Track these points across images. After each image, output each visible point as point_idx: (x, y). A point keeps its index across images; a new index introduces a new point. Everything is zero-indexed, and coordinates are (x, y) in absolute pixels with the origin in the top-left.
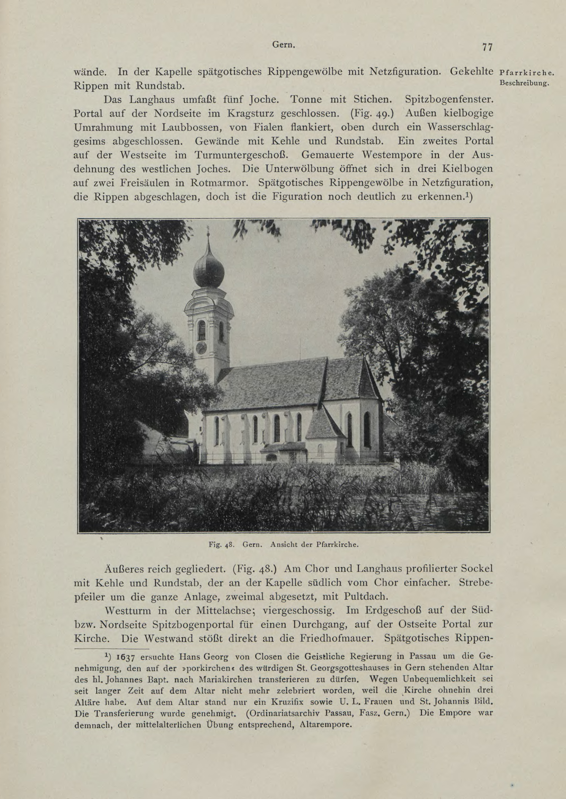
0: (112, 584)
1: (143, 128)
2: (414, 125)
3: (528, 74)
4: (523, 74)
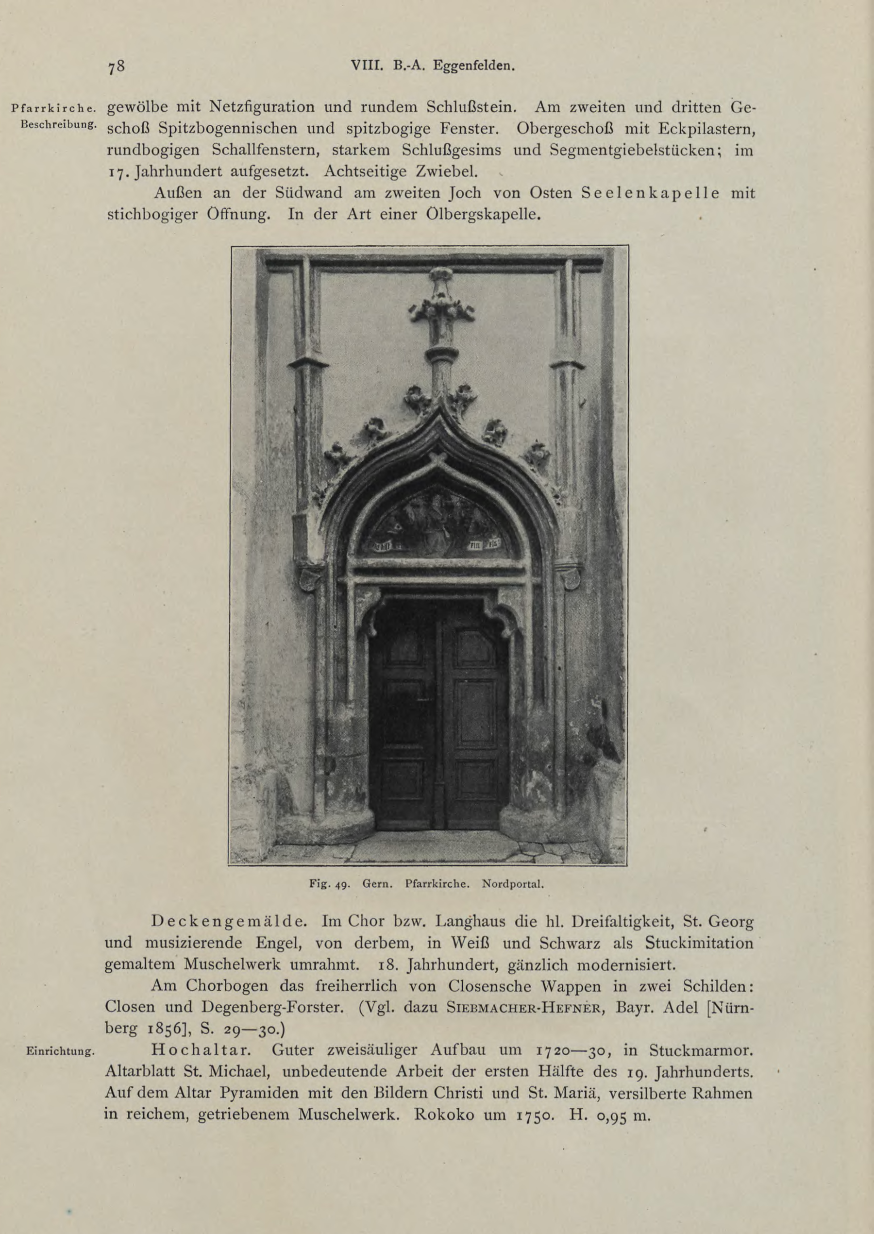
0: (449, 109)
2: (502, 103)
3: (55, 109)
4: (47, 110)
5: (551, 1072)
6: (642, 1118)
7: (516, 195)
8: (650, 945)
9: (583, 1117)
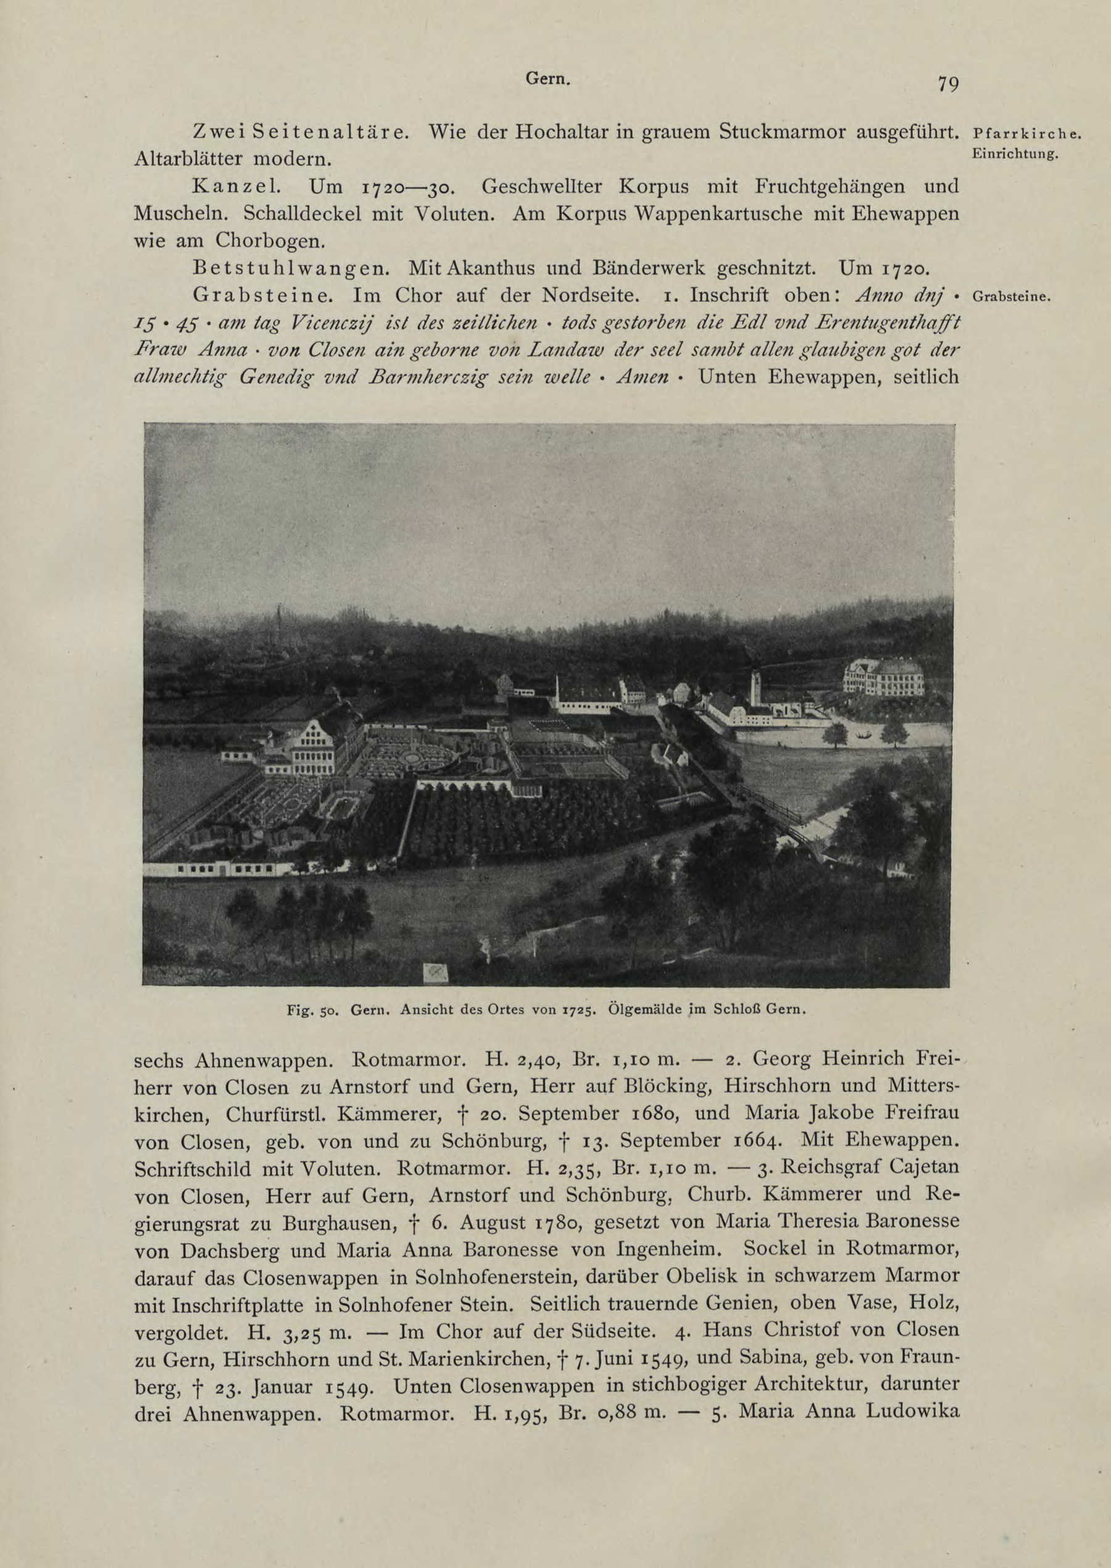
1: (335, 1333)
3: (1030, 135)
4: (1019, 135)
5: (720, 1332)
6: (341, 1335)
7: (879, 1332)
8: (726, 134)
9: (265, 1335)
